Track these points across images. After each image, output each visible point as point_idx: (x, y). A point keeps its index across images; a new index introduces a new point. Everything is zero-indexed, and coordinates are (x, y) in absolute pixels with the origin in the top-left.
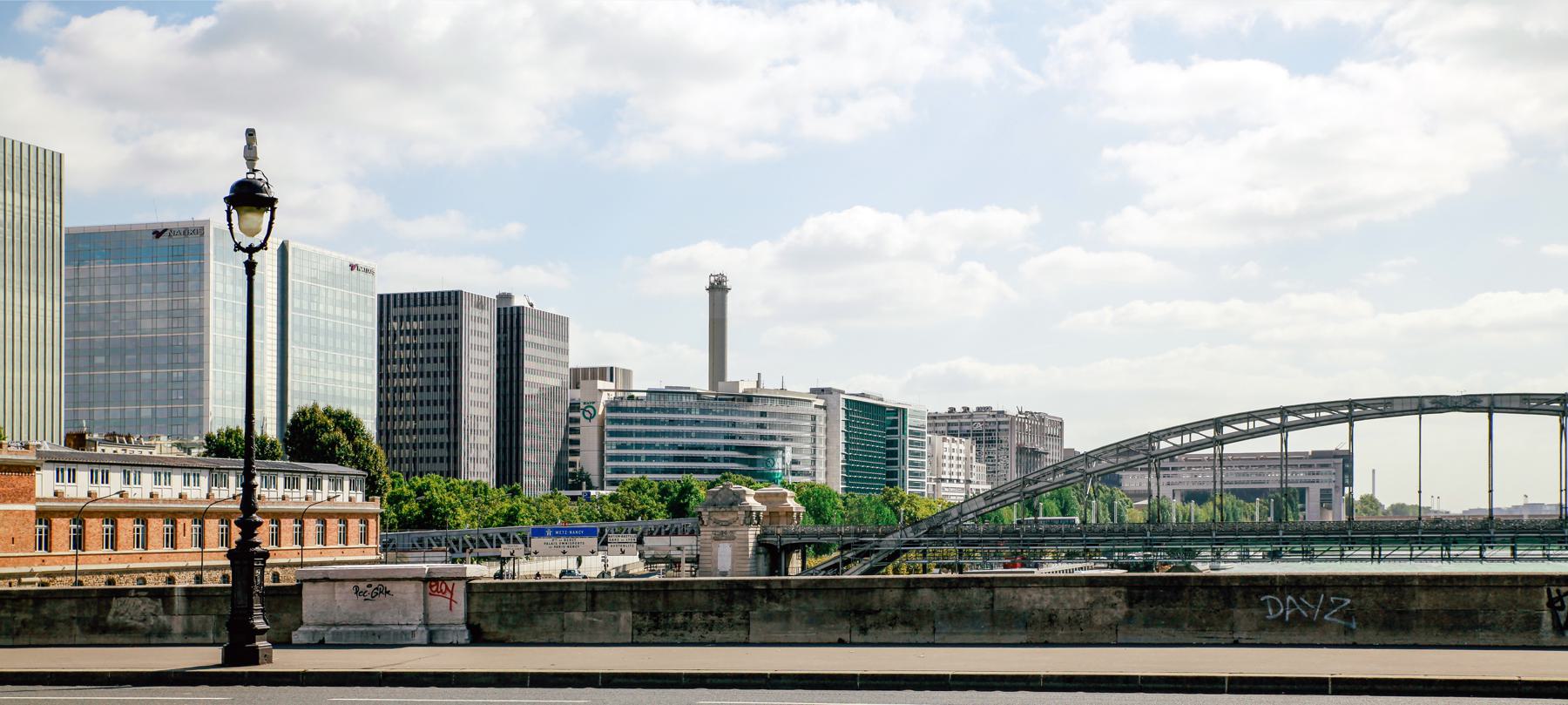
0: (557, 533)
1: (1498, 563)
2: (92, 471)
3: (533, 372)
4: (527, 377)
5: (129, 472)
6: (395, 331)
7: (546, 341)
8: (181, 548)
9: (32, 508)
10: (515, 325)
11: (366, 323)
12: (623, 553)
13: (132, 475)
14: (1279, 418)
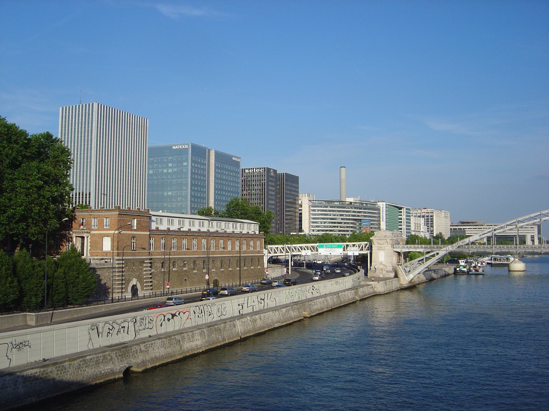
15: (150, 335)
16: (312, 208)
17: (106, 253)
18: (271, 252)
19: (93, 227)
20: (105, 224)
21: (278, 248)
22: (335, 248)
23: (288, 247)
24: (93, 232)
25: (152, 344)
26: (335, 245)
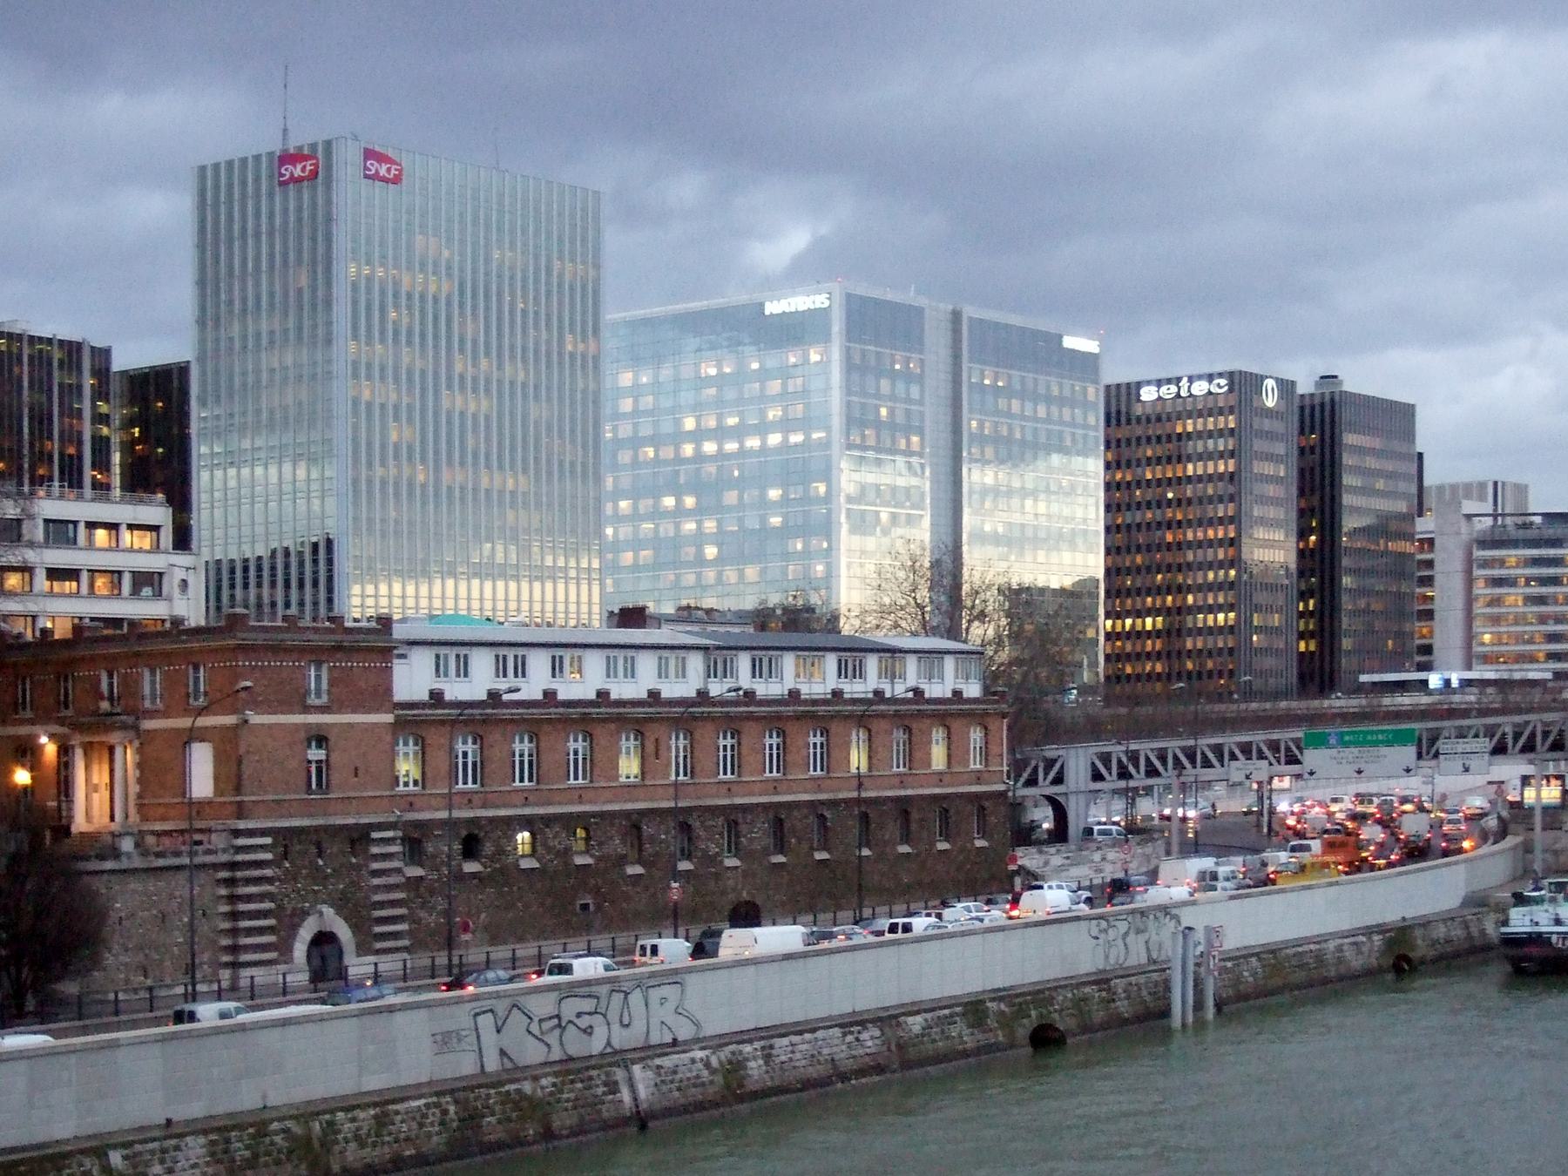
0: (1347, 738)
1: (269, 1000)
2: (660, 658)
3: (1355, 490)
4: (1347, 499)
5: (667, 658)
6: (369, 377)
7: (1377, 443)
8: (654, 778)
9: (389, 718)
10: (1327, 420)
11: (1086, 426)
12: (1467, 770)
13: (672, 663)
14: (767, 312)
15: (169, 1116)
16: (1479, 554)
17: (201, 807)
18: (1131, 769)
19: (147, 704)
20: (191, 689)
21: (1109, 754)
22: (1375, 744)
23: (1183, 749)
24: (148, 724)
25: (164, 1151)
26: (1383, 732)
